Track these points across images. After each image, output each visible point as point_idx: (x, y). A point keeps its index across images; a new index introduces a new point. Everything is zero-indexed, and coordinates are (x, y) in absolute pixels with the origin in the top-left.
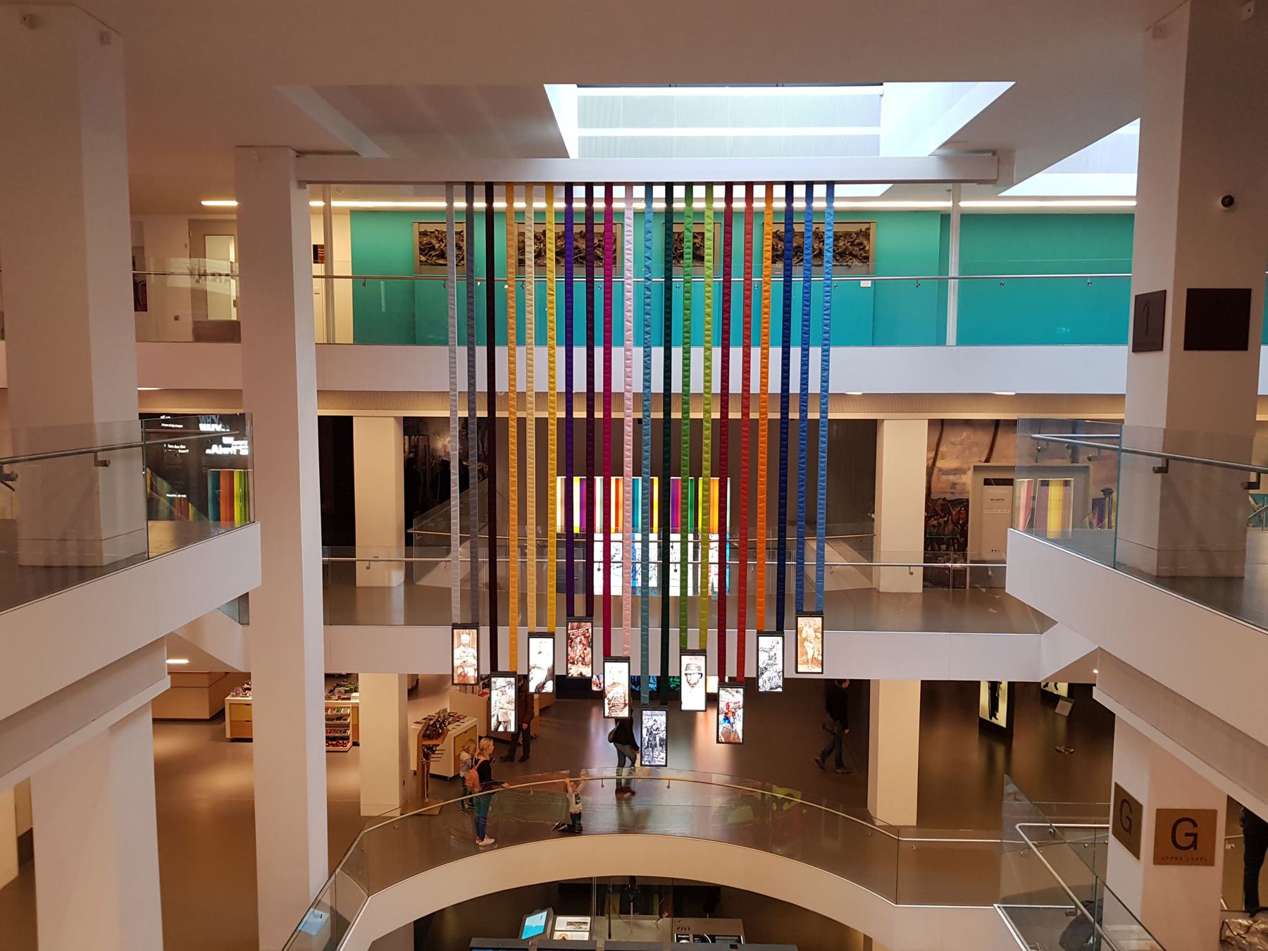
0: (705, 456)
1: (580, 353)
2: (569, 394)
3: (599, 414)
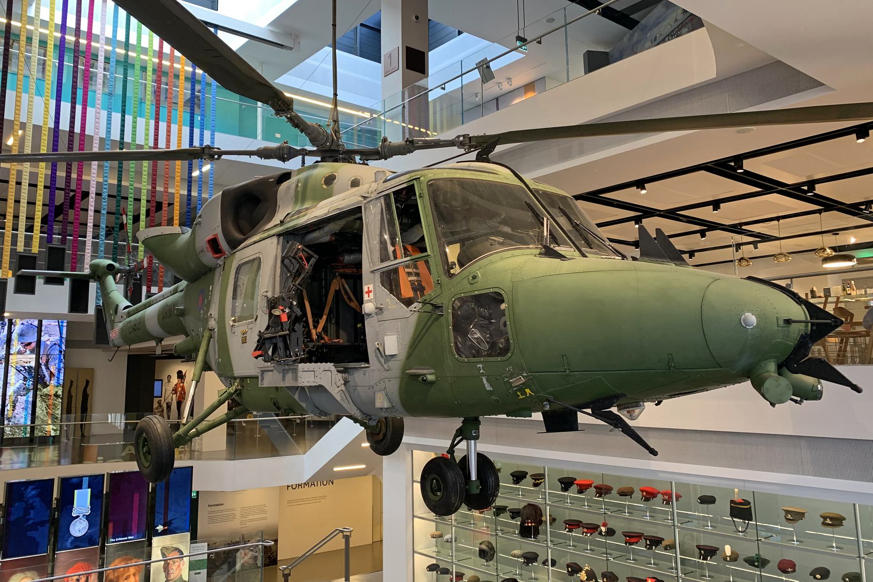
0: (144, 169)
1: (66, 107)
2: (63, 28)
3: (74, 176)
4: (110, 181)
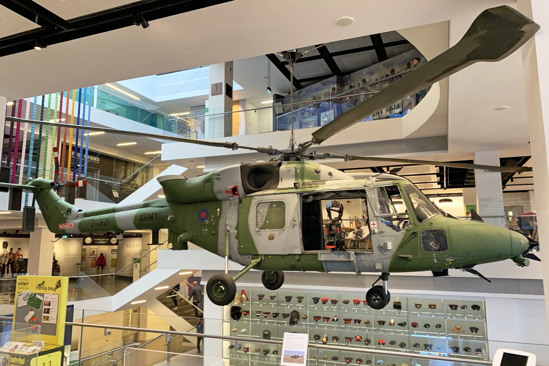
3: (15, 127)
4: (35, 133)
